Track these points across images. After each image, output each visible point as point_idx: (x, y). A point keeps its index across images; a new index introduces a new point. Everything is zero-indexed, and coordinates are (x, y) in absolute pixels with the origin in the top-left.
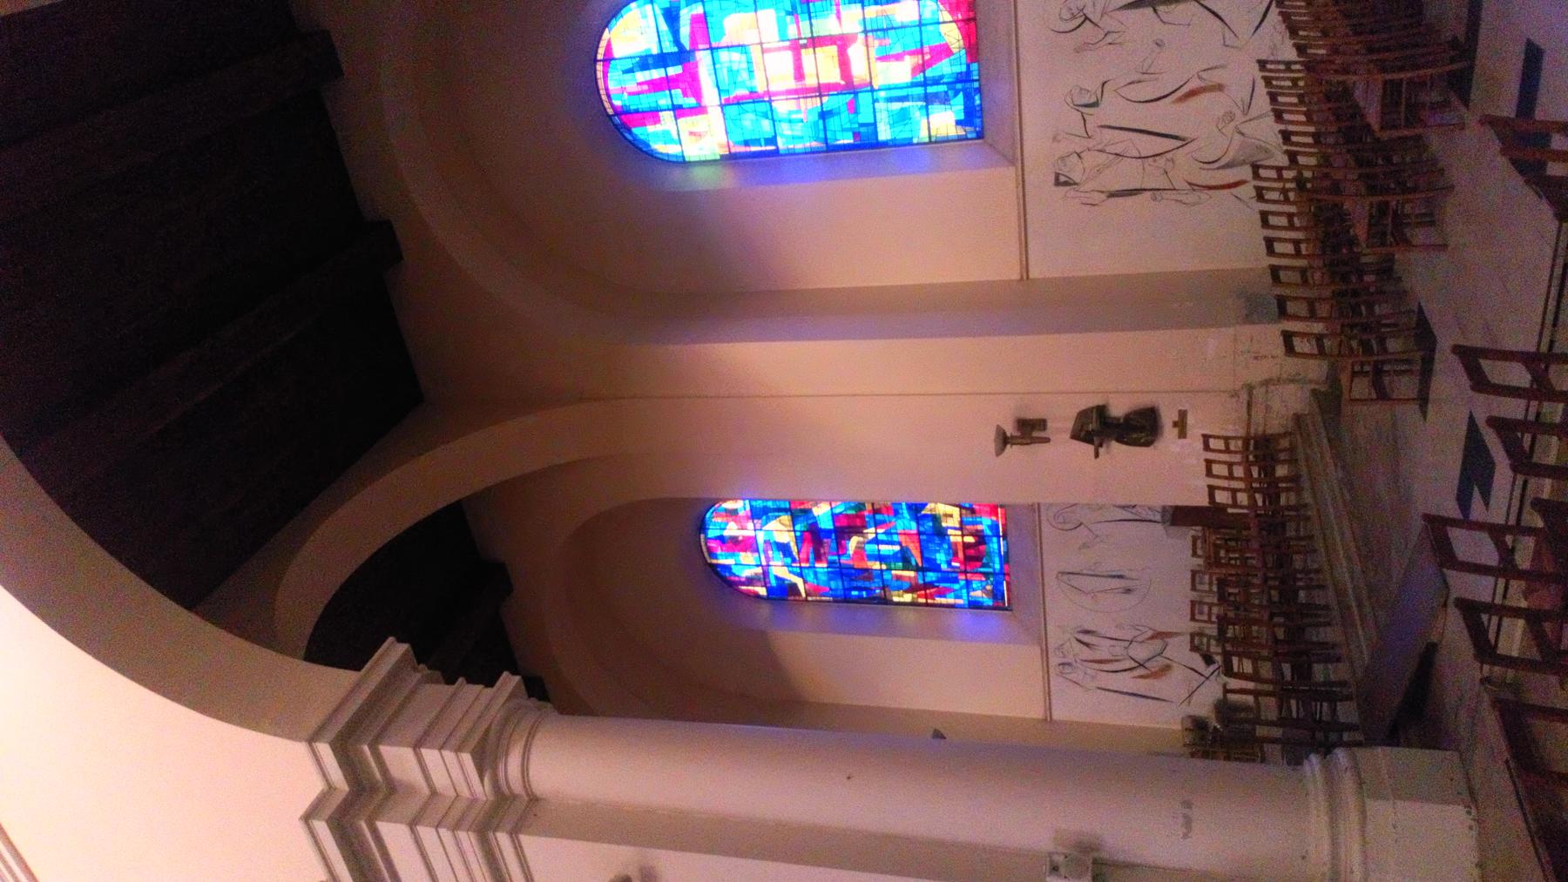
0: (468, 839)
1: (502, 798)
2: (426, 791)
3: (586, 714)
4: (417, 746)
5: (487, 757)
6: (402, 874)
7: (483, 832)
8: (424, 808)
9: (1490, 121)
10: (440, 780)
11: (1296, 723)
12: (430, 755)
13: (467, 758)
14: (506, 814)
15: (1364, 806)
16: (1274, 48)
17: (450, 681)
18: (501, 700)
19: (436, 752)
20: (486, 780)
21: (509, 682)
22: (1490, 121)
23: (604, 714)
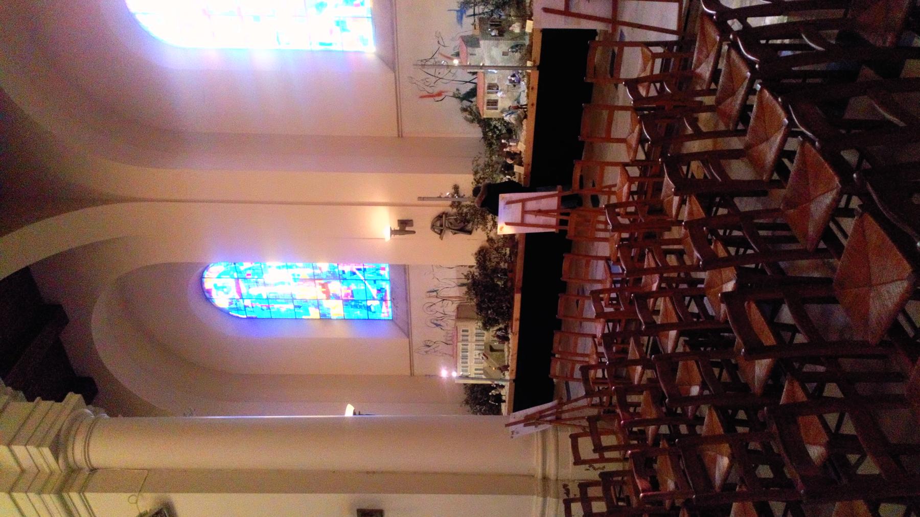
0: (51, 500)
1: (72, 471)
2: (48, 471)
3: (125, 415)
4: (25, 445)
5: (58, 448)
6: (26, 513)
7: (60, 492)
8: (47, 482)
9: (504, 401)
10: (26, 463)
11: (683, 418)
12: (19, 450)
13: (46, 451)
14: (73, 479)
15: (14, 501)
16: (716, 125)
17: (30, 398)
18: (67, 412)
19: (23, 448)
20: (61, 461)
21: (73, 398)
22: (504, 401)
23: (359, 472)
